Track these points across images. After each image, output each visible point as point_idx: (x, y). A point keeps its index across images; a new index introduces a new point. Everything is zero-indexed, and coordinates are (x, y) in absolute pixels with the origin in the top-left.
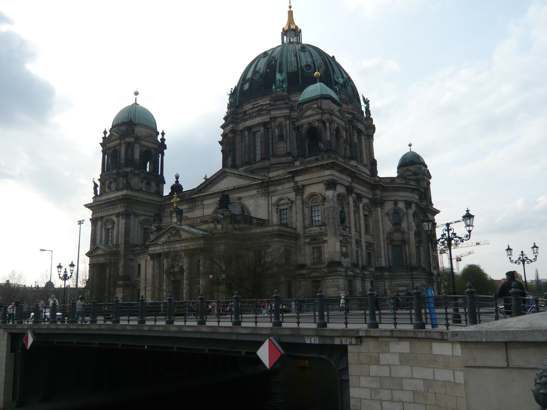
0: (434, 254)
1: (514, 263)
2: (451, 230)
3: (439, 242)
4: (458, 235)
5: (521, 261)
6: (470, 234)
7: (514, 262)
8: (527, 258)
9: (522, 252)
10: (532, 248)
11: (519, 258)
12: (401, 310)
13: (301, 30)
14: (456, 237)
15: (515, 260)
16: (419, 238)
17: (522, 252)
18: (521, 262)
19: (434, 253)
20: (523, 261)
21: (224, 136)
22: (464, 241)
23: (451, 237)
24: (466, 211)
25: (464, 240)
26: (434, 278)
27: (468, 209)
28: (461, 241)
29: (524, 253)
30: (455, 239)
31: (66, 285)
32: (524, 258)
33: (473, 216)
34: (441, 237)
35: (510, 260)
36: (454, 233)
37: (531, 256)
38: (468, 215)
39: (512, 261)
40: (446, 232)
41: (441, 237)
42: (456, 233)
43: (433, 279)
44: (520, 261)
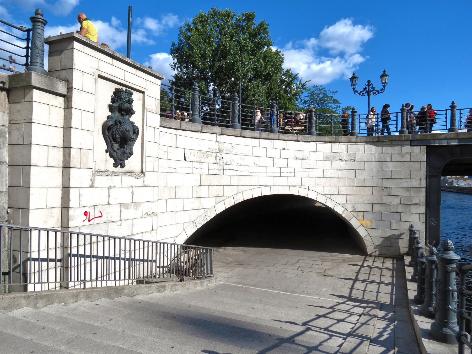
2: (371, 85)
4: (376, 89)
5: (367, 92)
6: (384, 88)
7: (358, 93)
8: (374, 88)
9: (369, 81)
11: (364, 89)
12: (177, 279)
14: (374, 90)
15: (359, 91)
17: (369, 81)
18: (366, 94)
20: (368, 92)
24: (383, 71)
25: (379, 92)
30: (373, 91)
32: (370, 88)
37: (378, 87)
39: (356, 92)
40: (367, 87)
44: (365, 92)
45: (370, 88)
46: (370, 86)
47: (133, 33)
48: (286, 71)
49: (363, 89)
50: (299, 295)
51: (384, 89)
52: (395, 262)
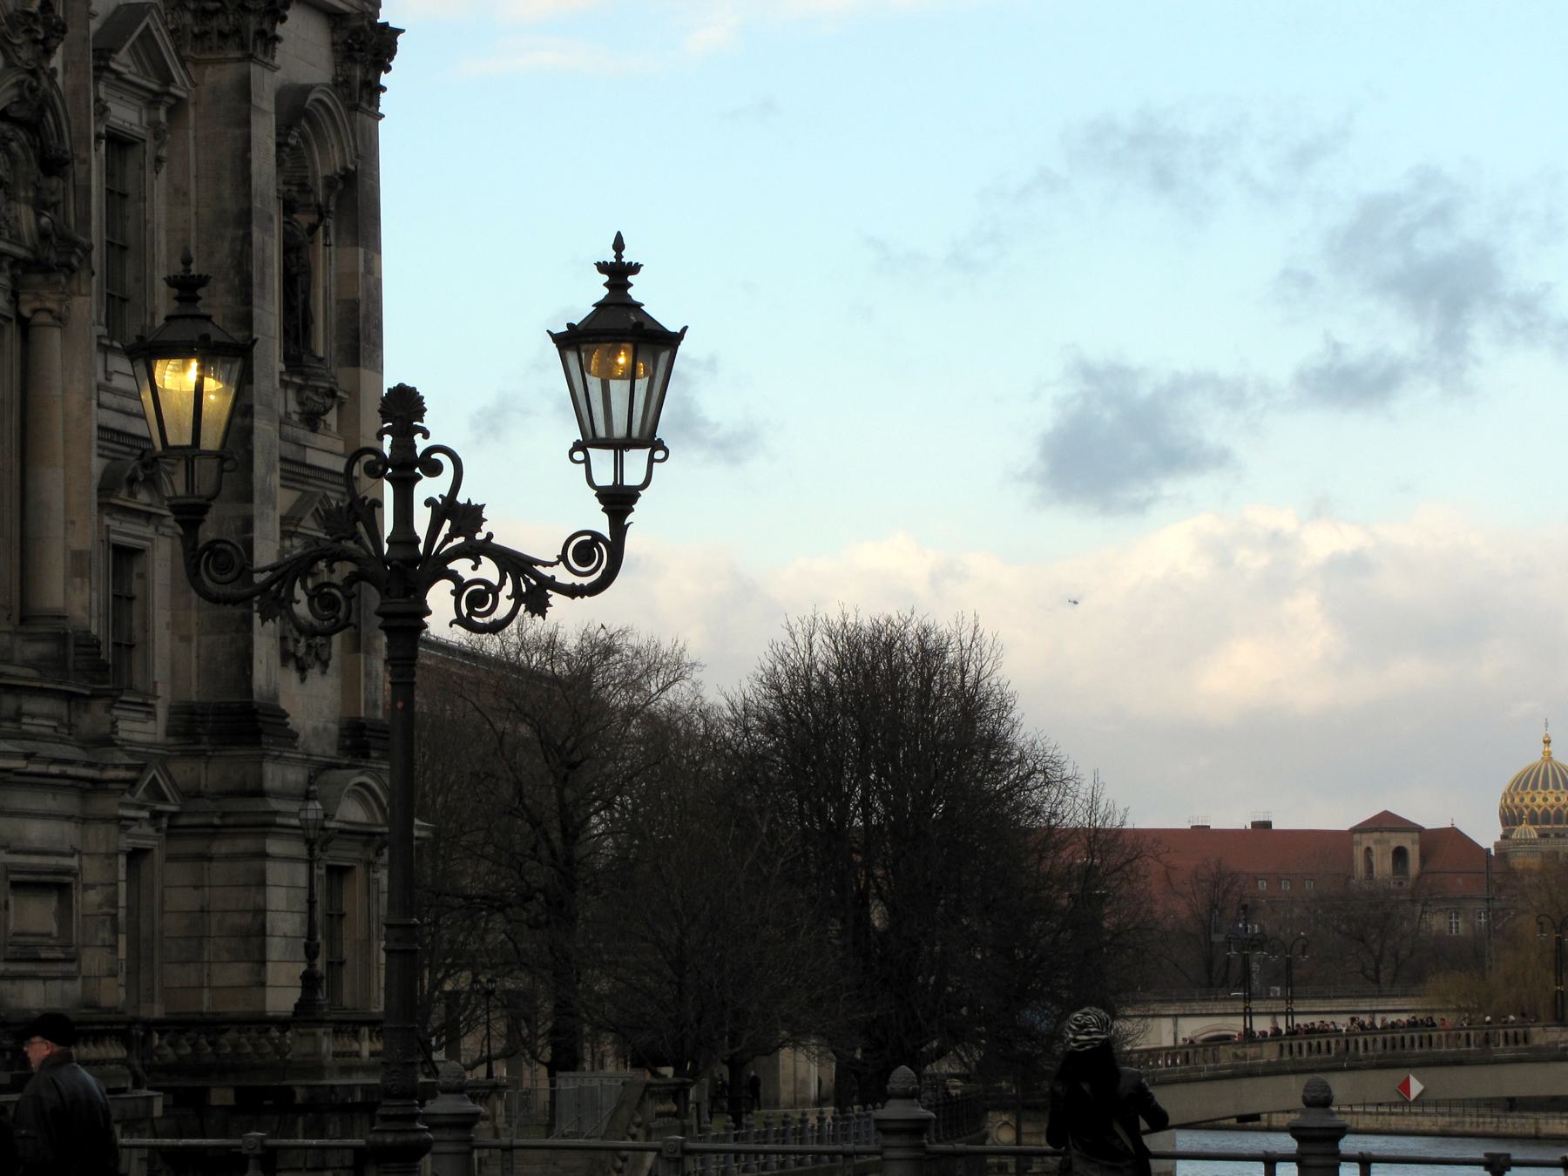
0: (314, 458)
2: (434, 469)
4: (500, 527)
13: (593, 306)
14: (475, 551)
16: (40, 206)
19: (319, 440)
22: (555, 599)
23: (421, 547)
24: (602, 267)
25: (551, 583)
26: (280, 775)
27: (619, 245)
28: (517, 595)
29: (428, 422)
30: (462, 567)
32: (422, 520)
33: (670, 341)
36: (462, 498)
42: (479, 509)
43: (260, 793)
44: (344, 569)
45: (422, 520)
46: (428, 488)
47: (188, 393)
48: (211, 506)
50: (183, 1142)
51: (617, 549)
52: (672, 1088)
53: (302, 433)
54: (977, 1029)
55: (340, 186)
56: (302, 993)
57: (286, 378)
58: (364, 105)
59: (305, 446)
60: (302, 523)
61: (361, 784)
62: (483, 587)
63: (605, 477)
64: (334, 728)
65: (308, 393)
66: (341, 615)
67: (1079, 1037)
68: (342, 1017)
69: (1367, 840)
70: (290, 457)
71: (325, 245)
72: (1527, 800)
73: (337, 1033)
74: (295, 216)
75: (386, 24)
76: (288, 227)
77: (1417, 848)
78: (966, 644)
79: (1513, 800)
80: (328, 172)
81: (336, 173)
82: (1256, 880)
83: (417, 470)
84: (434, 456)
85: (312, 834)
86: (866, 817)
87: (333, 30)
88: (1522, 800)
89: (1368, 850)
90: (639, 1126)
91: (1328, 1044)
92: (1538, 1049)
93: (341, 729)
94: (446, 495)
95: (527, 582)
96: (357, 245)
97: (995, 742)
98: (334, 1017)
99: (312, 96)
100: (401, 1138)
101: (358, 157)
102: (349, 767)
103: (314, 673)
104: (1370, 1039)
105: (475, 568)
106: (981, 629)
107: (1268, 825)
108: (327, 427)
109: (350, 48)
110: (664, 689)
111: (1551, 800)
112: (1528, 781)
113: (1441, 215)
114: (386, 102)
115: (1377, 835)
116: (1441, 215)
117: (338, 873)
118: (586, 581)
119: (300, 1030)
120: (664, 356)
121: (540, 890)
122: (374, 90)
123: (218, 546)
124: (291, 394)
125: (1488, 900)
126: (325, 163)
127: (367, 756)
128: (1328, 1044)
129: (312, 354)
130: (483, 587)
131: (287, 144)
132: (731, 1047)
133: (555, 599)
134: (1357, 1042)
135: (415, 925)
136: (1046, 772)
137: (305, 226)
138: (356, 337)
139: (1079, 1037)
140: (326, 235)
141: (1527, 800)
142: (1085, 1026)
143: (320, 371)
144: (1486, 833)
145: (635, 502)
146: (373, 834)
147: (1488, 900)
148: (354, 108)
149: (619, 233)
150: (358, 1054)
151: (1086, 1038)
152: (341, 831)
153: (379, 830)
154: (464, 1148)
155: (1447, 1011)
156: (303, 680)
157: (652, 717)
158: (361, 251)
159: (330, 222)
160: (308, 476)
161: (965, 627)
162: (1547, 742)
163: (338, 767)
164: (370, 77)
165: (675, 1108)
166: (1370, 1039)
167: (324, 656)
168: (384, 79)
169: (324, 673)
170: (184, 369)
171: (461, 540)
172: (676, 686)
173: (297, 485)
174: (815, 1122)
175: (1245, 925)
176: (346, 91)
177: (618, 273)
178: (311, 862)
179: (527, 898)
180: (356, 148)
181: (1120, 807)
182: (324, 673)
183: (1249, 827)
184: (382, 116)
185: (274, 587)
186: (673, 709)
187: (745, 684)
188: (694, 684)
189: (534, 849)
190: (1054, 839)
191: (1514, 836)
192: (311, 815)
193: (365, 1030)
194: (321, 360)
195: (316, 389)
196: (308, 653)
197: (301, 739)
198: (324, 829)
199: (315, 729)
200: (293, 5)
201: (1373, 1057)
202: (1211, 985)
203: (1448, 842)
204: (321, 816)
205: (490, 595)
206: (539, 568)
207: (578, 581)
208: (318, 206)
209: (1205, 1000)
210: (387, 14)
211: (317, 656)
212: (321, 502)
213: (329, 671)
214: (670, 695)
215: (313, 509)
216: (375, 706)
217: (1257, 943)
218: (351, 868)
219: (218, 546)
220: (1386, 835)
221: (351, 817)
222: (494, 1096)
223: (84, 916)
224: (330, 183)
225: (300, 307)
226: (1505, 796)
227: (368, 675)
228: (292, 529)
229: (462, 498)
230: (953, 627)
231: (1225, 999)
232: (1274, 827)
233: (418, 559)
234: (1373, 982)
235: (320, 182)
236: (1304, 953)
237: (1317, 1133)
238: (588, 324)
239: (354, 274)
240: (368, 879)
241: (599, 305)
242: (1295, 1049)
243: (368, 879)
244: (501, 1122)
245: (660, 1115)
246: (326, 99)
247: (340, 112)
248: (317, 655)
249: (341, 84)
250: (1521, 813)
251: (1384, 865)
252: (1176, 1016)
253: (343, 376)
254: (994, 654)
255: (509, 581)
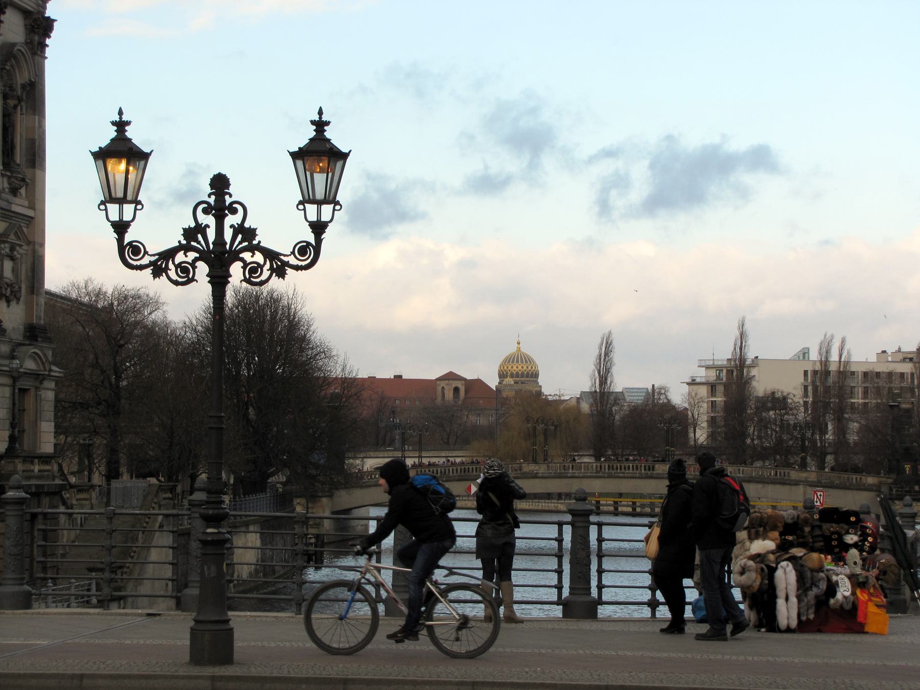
0: (15, 208)
1: (149, 271)
2: (234, 211)
3: (171, 266)
4: (264, 239)
5: (204, 256)
7: (146, 260)
9: (220, 183)
10: (295, 156)
14: (252, 249)
15: (156, 245)
17: (220, 183)
19: (17, 200)
21: (43, 51)
22: (289, 271)
23: (228, 247)
25: (287, 264)
28: (272, 269)
29: (231, 190)
30: (247, 256)
31: (454, 523)
32: (228, 234)
33: (344, 156)
34: (184, 242)
35: (120, 240)
36: (247, 225)
38: (317, 146)
40: (209, 220)
41: (184, 242)
42: (255, 230)
44: (192, 255)
46: (231, 220)
49: (175, 238)
53: (10, 197)
54: (907, 472)
55: (28, 88)
56: (9, 444)
57: (3, 172)
58: (39, 53)
59: (11, 203)
60: (10, 237)
61: (34, 353)
62: (256, 265)
63: (313, 217)
64: (22, 327)
65: (13, 180)
66: (191, 276)
67: (489, 471)
68: (26, 455)
69: (443, 384)
70: (5, 207)
71: (21, 114)
72: (510, 368)
73: (24, 461)
74: (8, 101)
75: (49, 17)
76: (5, 106)
77: (463, 387)
78: (291, 297)
79: (504, 368)
80: (23, 82)
81: (26, 82)
82: (395, 400)
83: (226, 212)
84: (234, 206)
85: (15, 374)
86: (249, 370)
87: (25, 19)
88: (508, 367)
89: (443, 388)
90: (155, 503)
91: (437, 470)
92: (525, 473)
93: (25, 328)
94: (239, 223)
95: (276, 263)
96: (34, 114)
97: (304, 339)
98: (23, 454)
99: (17, 47)
100: (216, 512)
101: (36, 75)
102: (29, 345)
103: (13, 303)
104: (455, 468)
105: (252, 256)
106: (296, 290)
107: (400, 377)
108: (21, 194)
109: (33, 27)
110: (150, 313)
111: (520, 368)
112: (510, 360)
113: (534, 111)
114: (48, 52)
115: (447, 382)
116: (534, 111)
117: (23, 391)
118: (304, 263)
119: (9, 460)
120: (339, 164)
121: (104, 400)
122: (43, 46)
123: (134, 244)
124: (5, 180)
125: (496, 410)
126: (21, 78)
127: (37, 340)
128: (437, 470)
129: (14, 162)
130: (256, 265)
131: (5, 69)
132: (192, 470)
133: (289, 271)
134: (449, 470)
135: (223, 417)
136: (326, 353)
137: (12, 105)
138: (34, 155)
139: (489, 471)
140: (21, 110)
141: (510, 368)
142: (492, 466)
143: (19, 170)
144: (493, 382)
145: (326, 228)
146: (39, 375)
147: (496, 410)
148: (34, 54)
149: (321, 107)
150: (33, 471)
151: (493, 472)
152: (25, 373)
153: (42, 373)
154: (20, 513)
155: (479, 456)
156: (8, 306)
157: (146, 327)
158: (37, 117)
159: (23, 104)
160: (13, 216)
161: (290, 289)
162: (519, 343)
163: (24, 345)
164: (42, 40)
165: (171, 496)
166: (455, 468)
167: (18, 296)
168: (48, 41)
169: (18, 303)
170: (120, 162)
171: (246, 244)
172: (156, 312)
173: (8, 220)
174: (228, 502)
175: (393, 419)
176: (31, 46)
177: (320, 125)
178: (13, 386)
179: (99, 404)
180: (35, 71)
181: (355, 369)
182: (18, 303)
183: (392, 377)
184: (46, 58)
185: (159, 263)
186: (154, 323)
187: (197, 313)
188: (164, 312)
189: (102, 382)
190: (327, 381)
191: (504, 383)
192: (14, 366)
193: (36, 461)
194: (19, 165)
195: (16, 178)
196: (11, 294)
197: (8, 332)
198: (19, 372)
199: (13, 329)
200: (8, 7)
201: (455, 476)
202: (378, 444)
203: (476, 385)
204: (19, 366)
205: (259, 269)
206: (282, 257)
207: (300, 263)
208: (18, 96)
209: (375, 451)
210: (50, 12)
211: (15, 296)
212: (18, 228)
213: (20, 302)
214: (153, 316)
215: (14, 231)
216: (40, 318)
217: (396, 426)
218: (29, 389)
219: (134, 244)
220: (451, 381)
221: (30, 367)
222: (91, 490)
223: (19, 410)
224: (23, 87)
225: (10, 141)
226: (500, 366)
227: (37, 305)
228: (5, 239)
229: (247, 225)
230: (285, 289)
231: (384, 451)
232: (403, 378)
233: (227, 252)
234: (447, 444)
235: (19, 87)
236: (427, 432)
237: (581, 512)
238: (308, 147)
239: (34, 128)
240: (36, 395)
241: (311, 140)
242: (455, 472)
243: (36, 395)
244: (94, 501)
245: (165, 499)
246: (23, 50)
247: (28, 55)
248: (15, 295)
249: (29, 43)
250: (507, 373)
251: (449, 395)
252: (363, 458)
253: (28, 172)
254: (302, 301)
255: (268, 262)
